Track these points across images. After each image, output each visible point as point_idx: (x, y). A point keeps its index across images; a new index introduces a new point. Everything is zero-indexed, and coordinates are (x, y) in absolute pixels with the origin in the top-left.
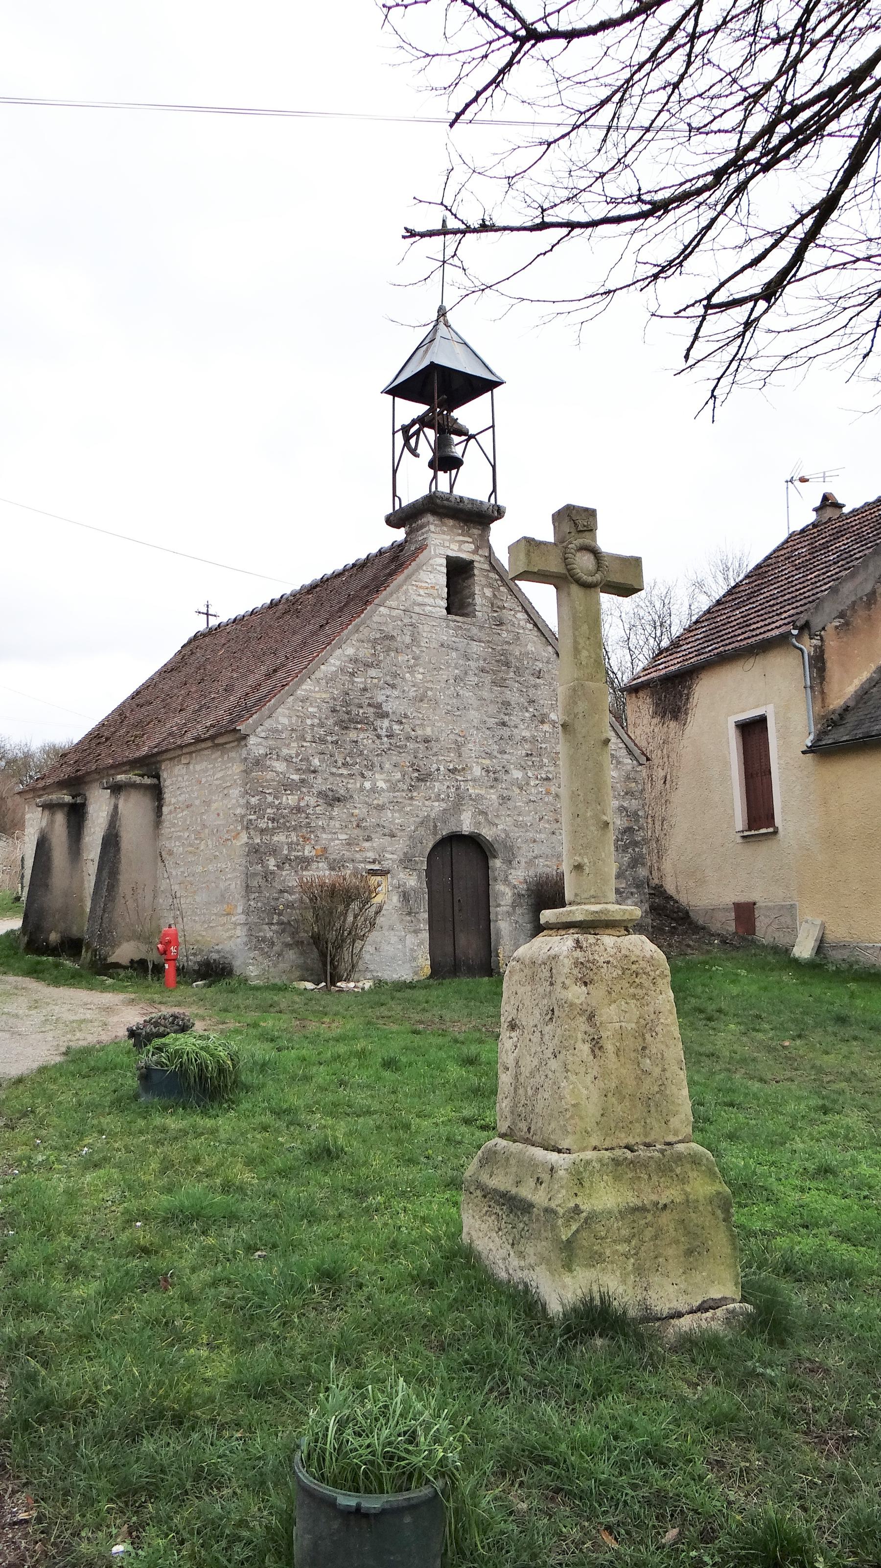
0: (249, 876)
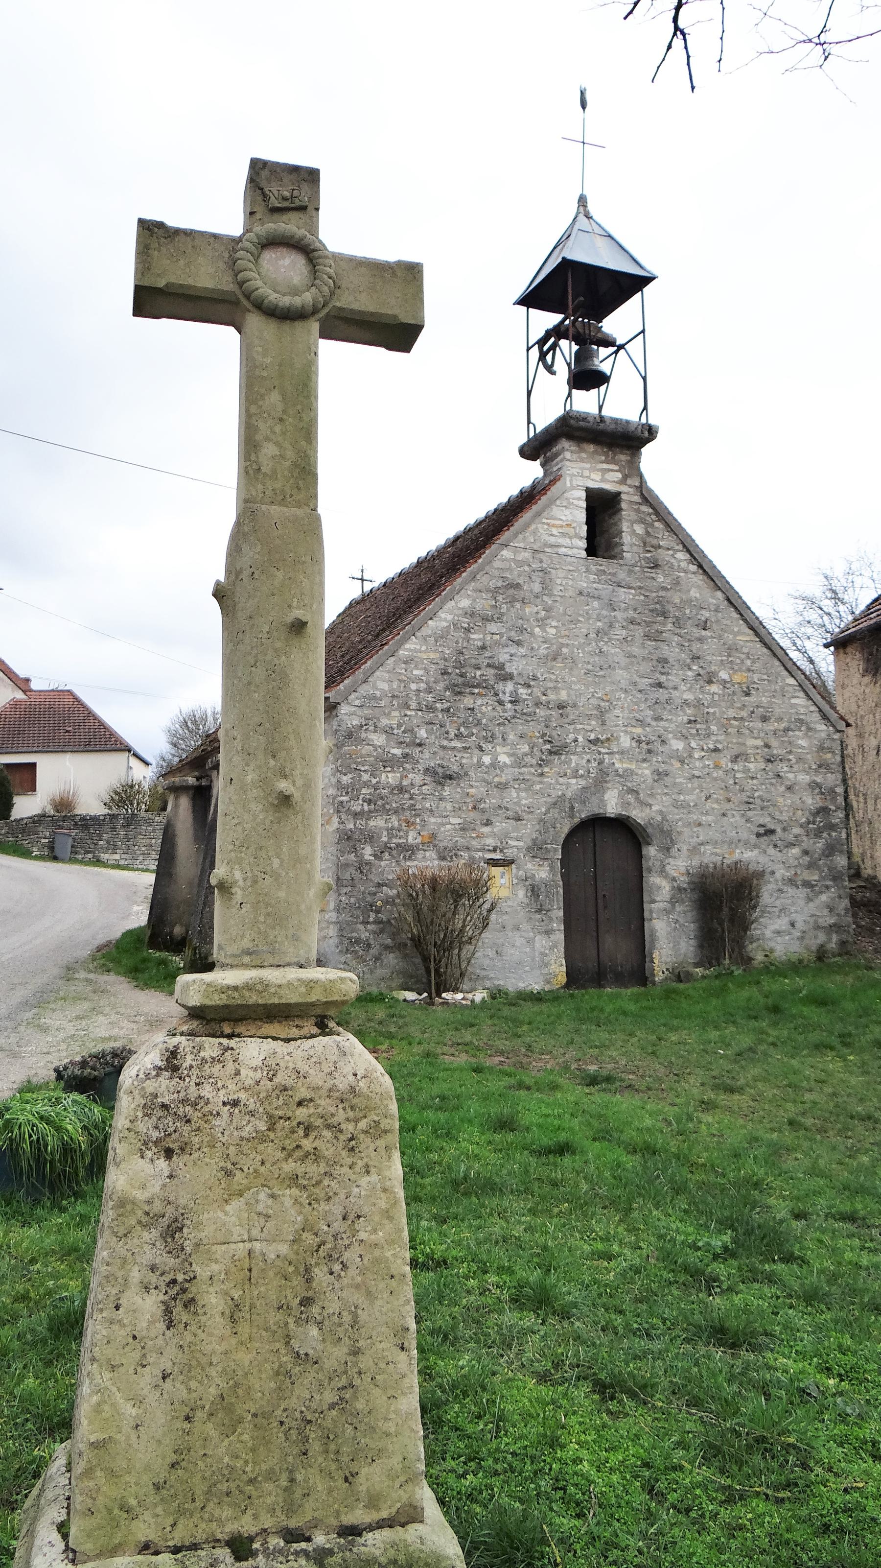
0: (342, 866)
